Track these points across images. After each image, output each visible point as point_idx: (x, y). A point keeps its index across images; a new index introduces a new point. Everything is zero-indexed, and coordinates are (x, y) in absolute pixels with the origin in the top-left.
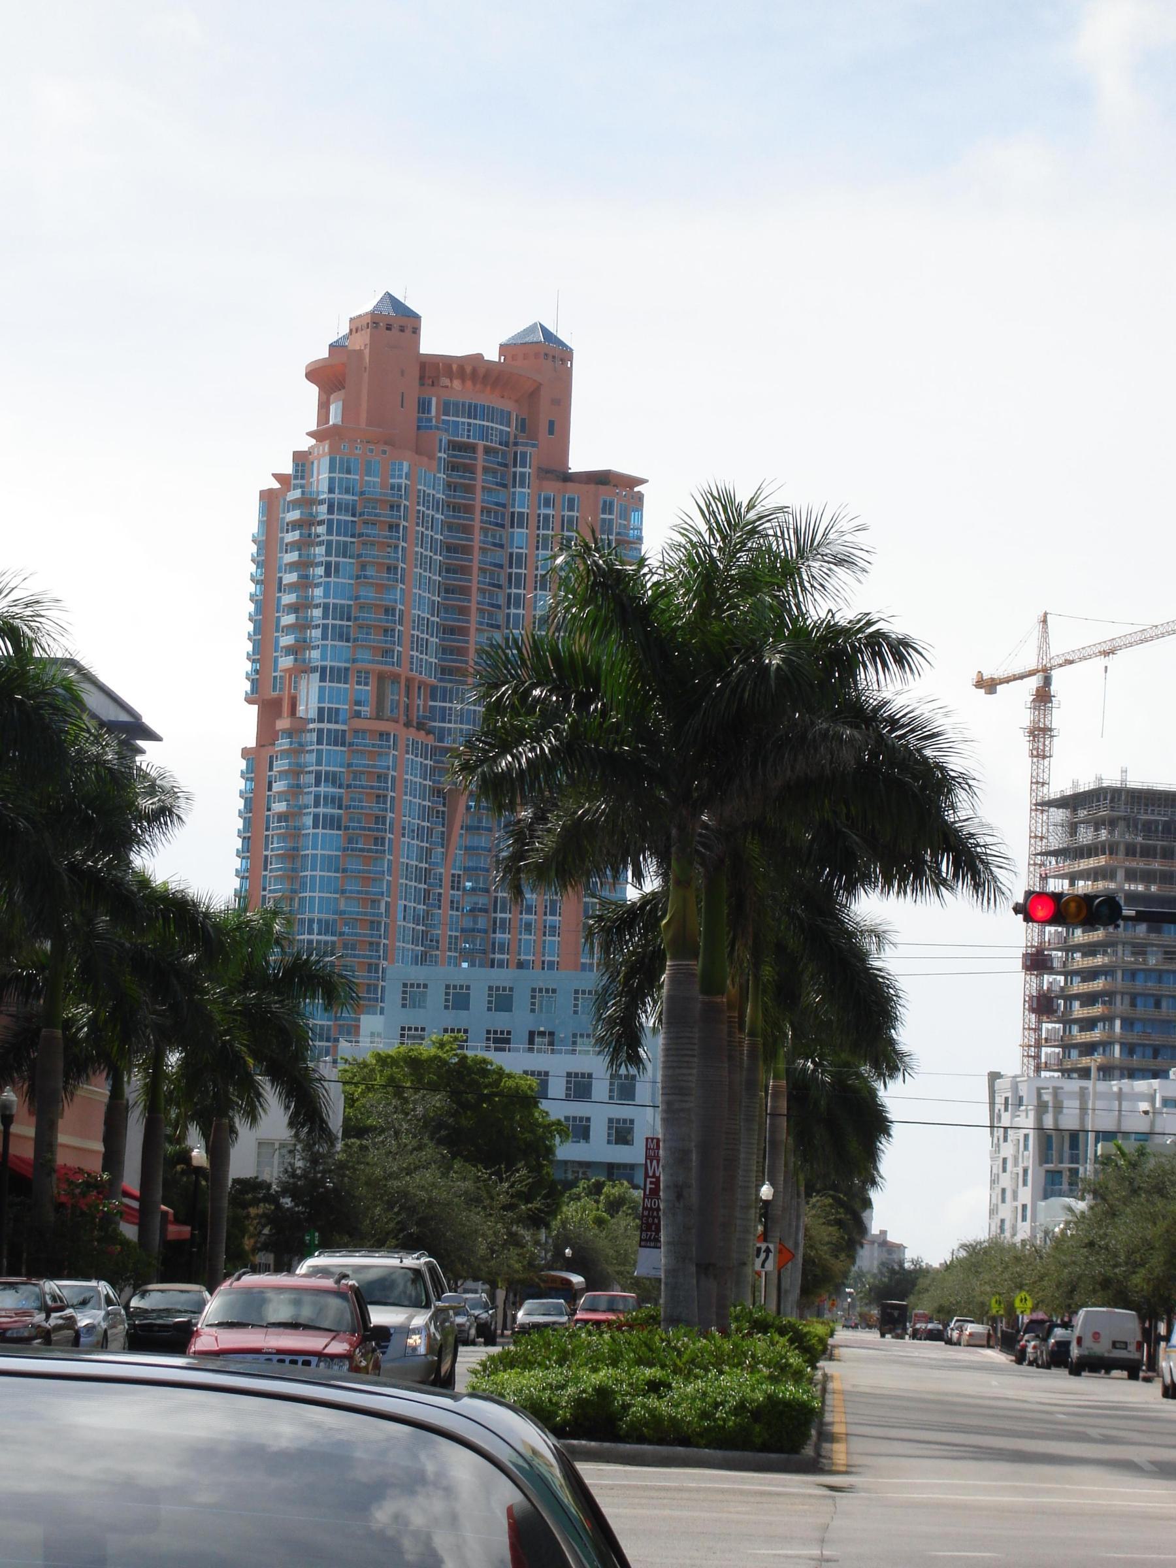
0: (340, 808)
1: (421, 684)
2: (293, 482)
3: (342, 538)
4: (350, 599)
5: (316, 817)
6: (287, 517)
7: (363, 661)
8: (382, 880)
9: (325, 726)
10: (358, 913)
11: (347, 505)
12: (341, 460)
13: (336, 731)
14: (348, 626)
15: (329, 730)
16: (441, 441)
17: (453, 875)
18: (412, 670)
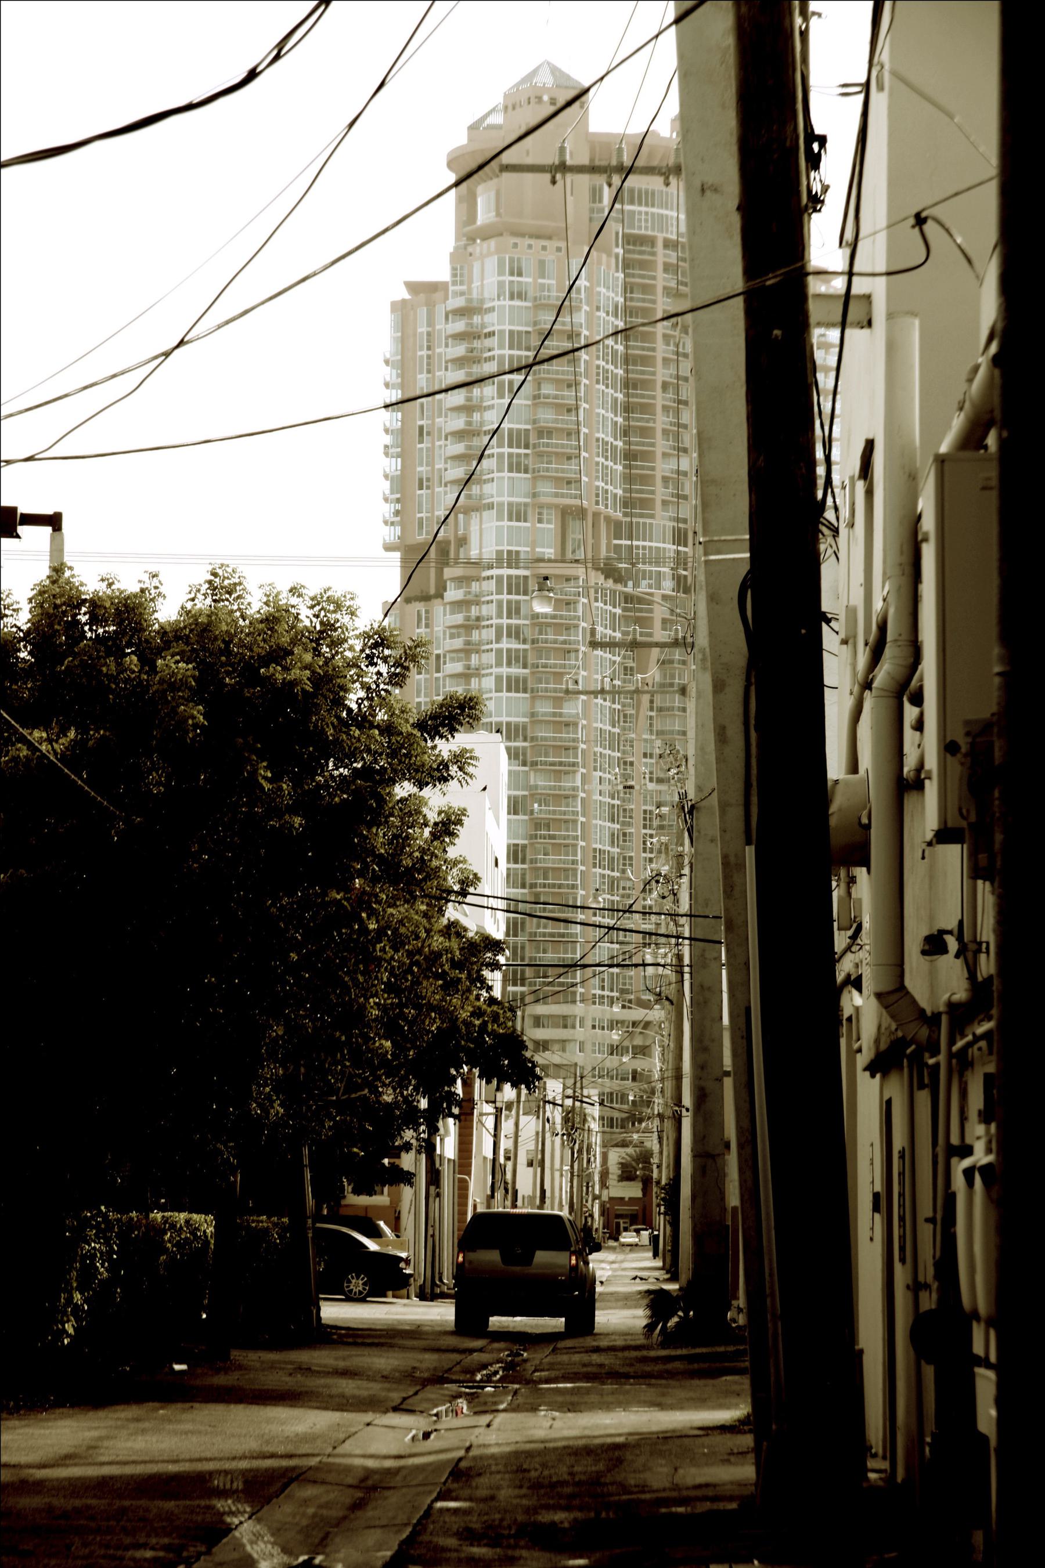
0: (525, 667)
1: (608, 519)
2: (451, 288)
3: (514, 597)
4: (527, 325)
5: (499, 678)
6: (451, 254)
7: (546, 494)
8: (575, 797)
9: (506, 572)
10: (550, 788)
11: (517, 680)
12: (512, 260)
13: (518, 577)
14: (526, 455)
15: (509, 577)
16: (617, 234)
17: (645, 812)
18: (597, 503)
